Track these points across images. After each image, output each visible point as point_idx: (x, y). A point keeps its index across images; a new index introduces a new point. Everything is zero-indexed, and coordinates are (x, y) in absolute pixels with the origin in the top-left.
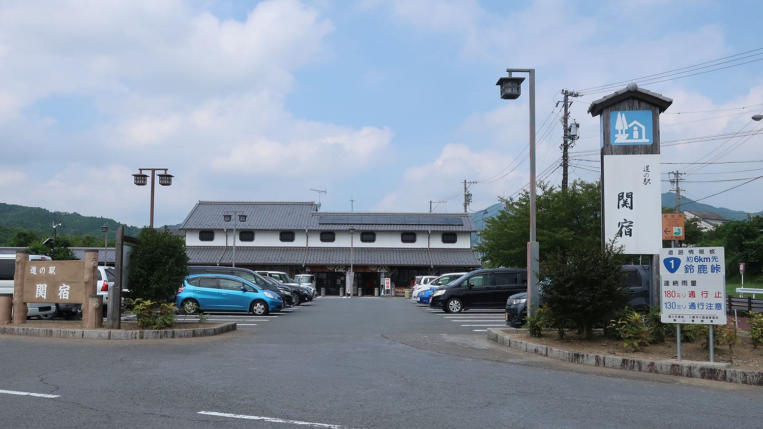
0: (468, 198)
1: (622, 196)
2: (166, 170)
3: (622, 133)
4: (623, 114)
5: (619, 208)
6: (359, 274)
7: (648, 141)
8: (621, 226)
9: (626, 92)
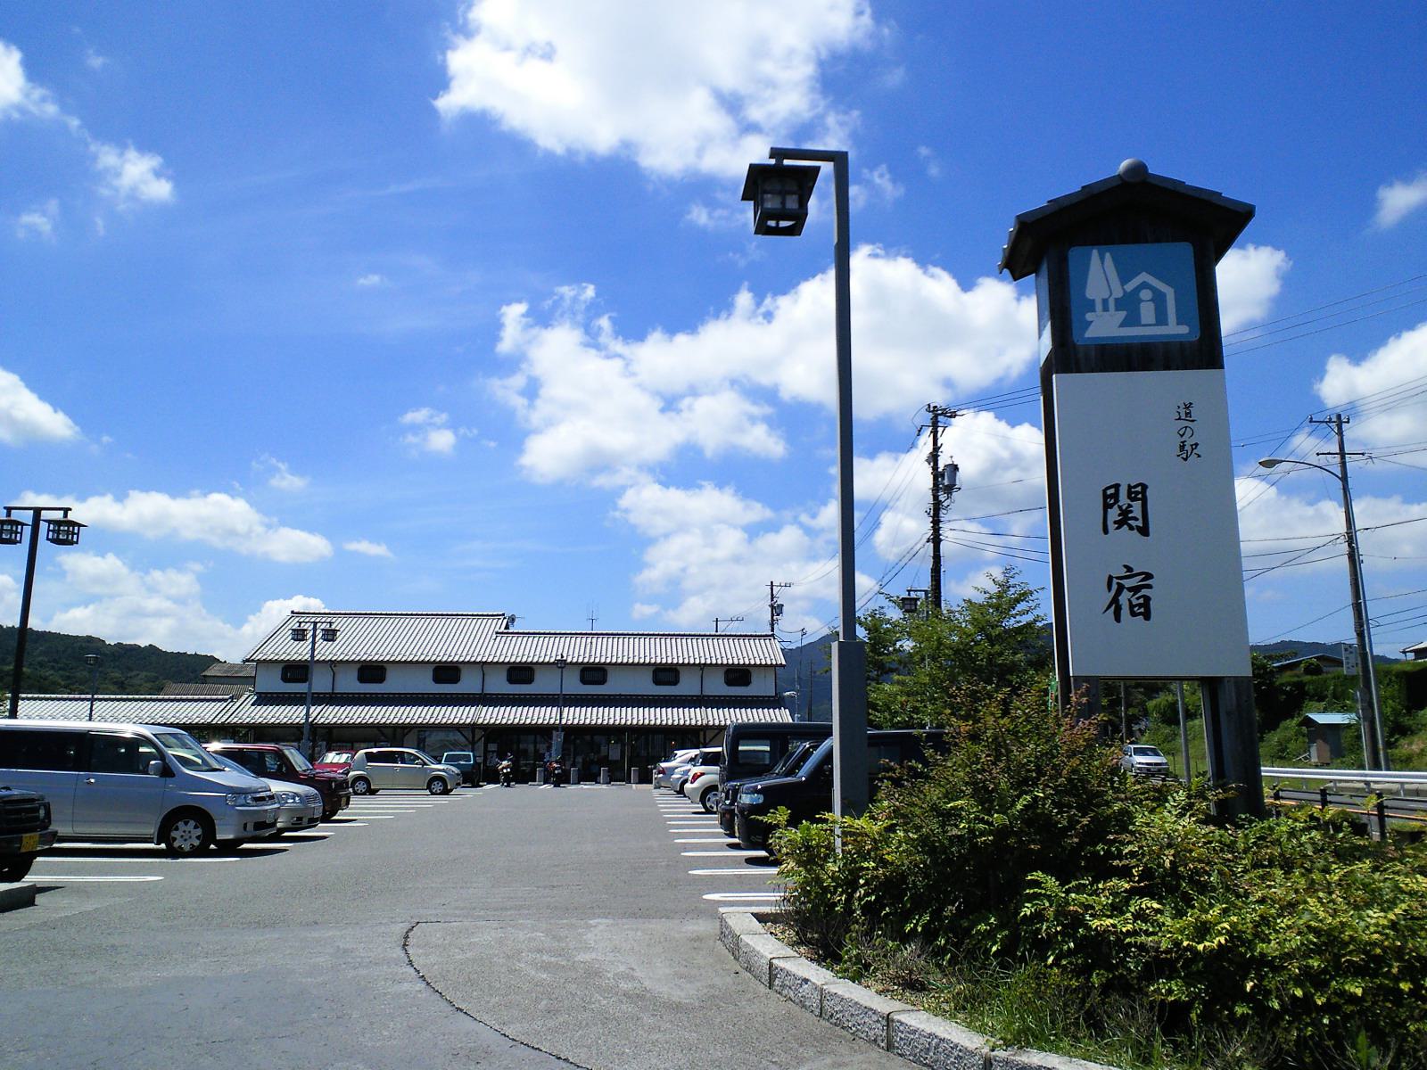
0: (777, 610)
1: (1116, 496)
2: (66, 510)
3: (1106, 309)
4: (1108, 255)
5: (1106, 531)
6: (489, 749)
7: (1184, 330)
8: (1115, 587)
9: (1118, 186)
